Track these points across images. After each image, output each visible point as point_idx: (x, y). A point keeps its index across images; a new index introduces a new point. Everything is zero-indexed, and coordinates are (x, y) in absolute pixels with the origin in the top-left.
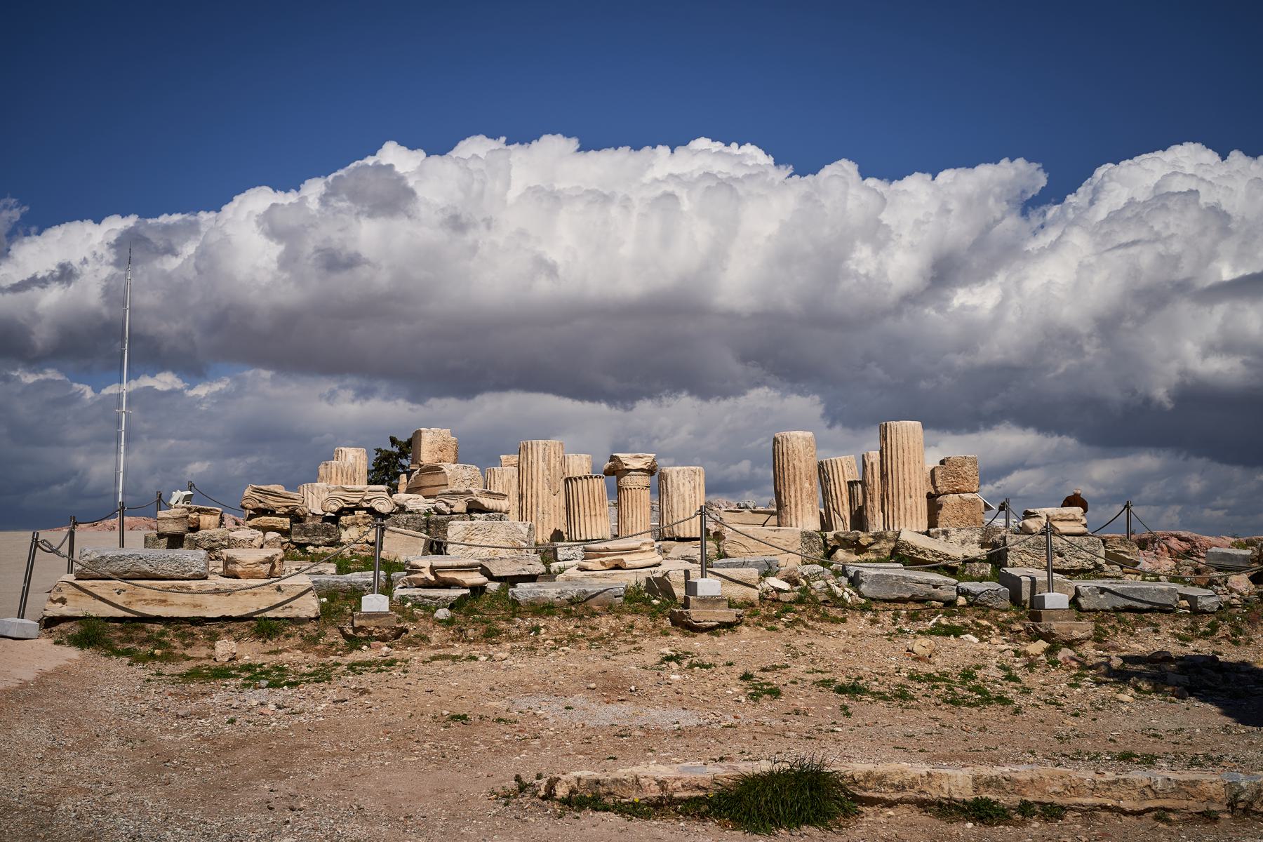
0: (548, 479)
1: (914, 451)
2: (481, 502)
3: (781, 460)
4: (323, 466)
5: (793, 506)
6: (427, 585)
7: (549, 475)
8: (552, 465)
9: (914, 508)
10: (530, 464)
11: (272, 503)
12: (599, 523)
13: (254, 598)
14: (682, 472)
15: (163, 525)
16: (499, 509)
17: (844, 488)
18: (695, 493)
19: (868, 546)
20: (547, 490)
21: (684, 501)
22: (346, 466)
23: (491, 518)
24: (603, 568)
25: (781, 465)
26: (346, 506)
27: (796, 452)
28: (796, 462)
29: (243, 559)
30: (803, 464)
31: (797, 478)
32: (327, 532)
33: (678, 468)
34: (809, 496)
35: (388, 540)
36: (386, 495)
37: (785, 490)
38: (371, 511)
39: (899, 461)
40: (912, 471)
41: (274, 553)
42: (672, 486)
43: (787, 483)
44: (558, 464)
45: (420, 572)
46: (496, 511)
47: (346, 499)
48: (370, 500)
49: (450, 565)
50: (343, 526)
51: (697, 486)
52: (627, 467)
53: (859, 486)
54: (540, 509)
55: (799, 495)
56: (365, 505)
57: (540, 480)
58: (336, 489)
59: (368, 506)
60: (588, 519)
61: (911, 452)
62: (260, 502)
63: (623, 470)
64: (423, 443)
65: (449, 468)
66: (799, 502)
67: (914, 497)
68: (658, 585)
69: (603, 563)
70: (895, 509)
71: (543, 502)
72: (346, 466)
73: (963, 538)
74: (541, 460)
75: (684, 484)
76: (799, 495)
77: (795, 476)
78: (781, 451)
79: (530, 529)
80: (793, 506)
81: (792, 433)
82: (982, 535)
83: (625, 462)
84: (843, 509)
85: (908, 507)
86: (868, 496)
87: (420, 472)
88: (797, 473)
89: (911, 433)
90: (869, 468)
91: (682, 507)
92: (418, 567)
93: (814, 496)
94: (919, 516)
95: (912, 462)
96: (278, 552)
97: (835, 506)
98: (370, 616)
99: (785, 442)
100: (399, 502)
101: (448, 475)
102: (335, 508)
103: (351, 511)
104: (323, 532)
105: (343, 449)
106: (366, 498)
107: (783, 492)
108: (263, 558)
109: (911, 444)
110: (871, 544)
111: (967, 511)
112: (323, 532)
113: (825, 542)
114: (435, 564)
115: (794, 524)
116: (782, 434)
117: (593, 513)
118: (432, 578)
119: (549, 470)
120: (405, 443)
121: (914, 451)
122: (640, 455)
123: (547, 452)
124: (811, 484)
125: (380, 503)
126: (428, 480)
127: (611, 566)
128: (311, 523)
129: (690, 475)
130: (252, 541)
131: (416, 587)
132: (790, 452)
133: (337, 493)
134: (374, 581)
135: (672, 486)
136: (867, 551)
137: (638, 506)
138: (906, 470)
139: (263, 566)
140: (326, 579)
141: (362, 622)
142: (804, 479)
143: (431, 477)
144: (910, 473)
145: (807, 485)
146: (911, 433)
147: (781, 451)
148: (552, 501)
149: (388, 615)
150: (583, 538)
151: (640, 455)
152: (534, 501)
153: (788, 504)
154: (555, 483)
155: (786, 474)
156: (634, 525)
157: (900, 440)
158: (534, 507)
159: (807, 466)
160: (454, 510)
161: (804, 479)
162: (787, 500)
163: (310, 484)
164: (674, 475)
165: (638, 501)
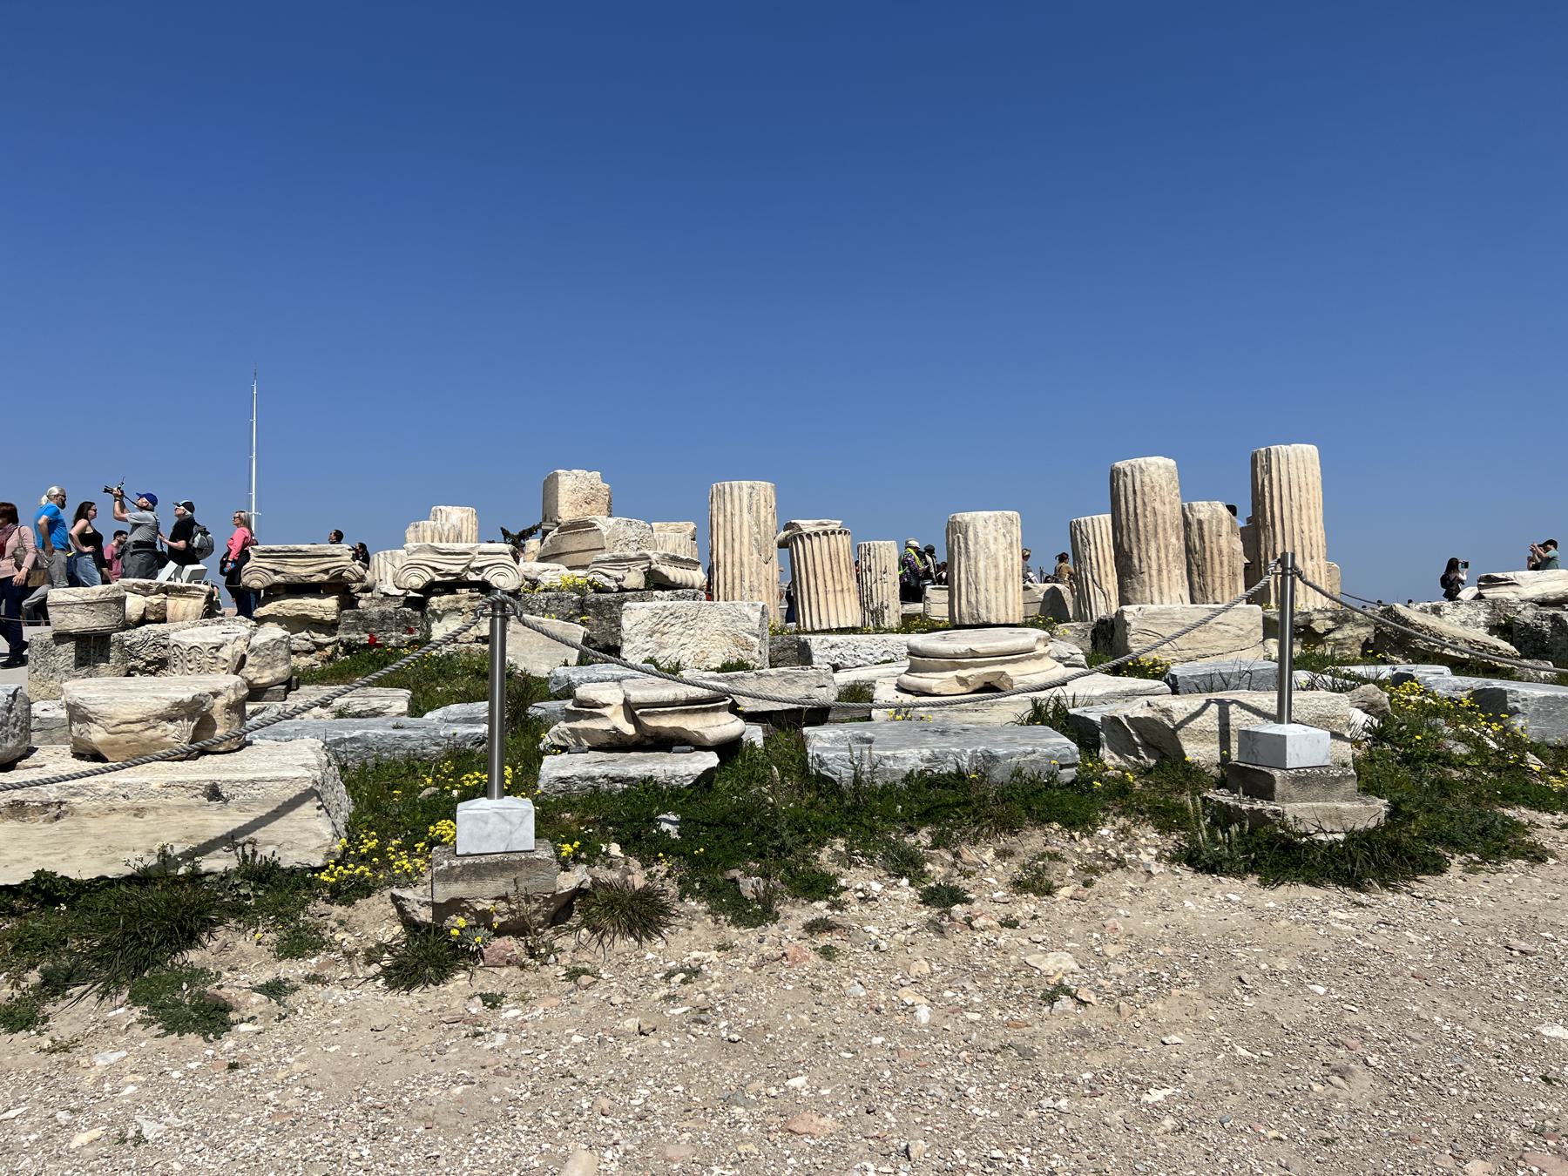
0: (756, 540)
2: (665, 573)
4: (411, 528)
5: (1154, 573)
6: (615, 744)
7: (759, 533)
8: (762, 519)
10: (729, 516)
11: (295, 570)
12: (847, 602)
13: (138, 825)
14: (993, 519)
15: (61, 616)
16: (690, 584)
18: (1012, 553)
20: (756, 555)
21: (996, 566)
22: (446, 528)
23: (684, 597)
24: (964, 690)
25: (1131, 510)
26: (438, 579)
27: (1157, 489)
28: (1158, 505)
29: (104, 709)
30: (1168, 507)
31: (1160, 530)
32: (406, 624)
33: (986, 514)
35: (515, 638)
36: (509, 559)
37: (1139, 549)
38: (485, 587)
41: (205, 689)
42: (976, 543)
43: (1142, 538)
44: (770, 517)
45: (600, 716)
46: (686, 587)
47: (439, 566)
48: (481, 569)
49: (671, 697)
50: (434, 612)
51: (1015, 542)
54: (746, 584)
55: (1163, 555)
56: (472, 577)
57: (746, 541)
58: (420, 550)
59: (479, 578)
60: (831, 596)
62: (276, 572)
65: (604, 523)
66: (1164, 566)
67: (1315, 559)
68: (1140, 735)
69: (962, 681)
71: (751, 573)
72: (446, 528)
73: (1463, 618)
74: (745, 510)
75: (996, 539)
76: (1163, 555)
77: (1156, 527)
78: (1130, 489)
79: (763, 613)
80: (1154, 573)
81: (1149, 459)
82: (1489, 614)
84: (1107, 582)
86: (1195, 568)
87: (559, 532)
88: (1160, 521)
89: (1309, 462)
90: (1195, 527)
92: (595, 705)
95: (1312, 506)
96: (220, 687)
97: (1096, 577)
98: (479, 870)
99: (1137, 474)
100: (529, 575)
101: (605, 534)
102: (418, 582)
103: (450, 587)
104: (398, 625)
105: (442, 508)
106: (474, 565)
107: (1135, 551)
108: (167, 703)
110: (1329, 631)
112: (398, 625)
114: (637, 696)
115: (1156, 599)
116: (1132, 461)
117: (838, 588)
118: (629, 729)
119: (758, 526)
120: (517, 536)
122: (825, 521)
124: (1178, 539)
125: (500, 574)
126: (572, 543)
127: (977, 687)
128: (377, 609)
129: (1005, 524)
130: (218, 649)
131: (591, 749)
132: (1147, 489)
133: (422, 556)
134: (491, 729)
135: (976, 543)
138: (1305, 517)
139: (171, 727)
140: (380, 732)
141: (458, 889)
142: (1170, 531)
143: (578, 538)
144: (1310, 523)
145: (1174, 540)
146: (1309, 462)
147: (1130, 489)
148: (763, 572)
149: (531, 863)
150: (825, 626)
151: (825, 521)
152: (737, 571)
153: (1145, 569)
154: (767, 545)
155: (1140, 523)
158: (737, 582)
160: (625, 584)
162: (1144, 564)
163: (388, 552)
164: (980, 525)
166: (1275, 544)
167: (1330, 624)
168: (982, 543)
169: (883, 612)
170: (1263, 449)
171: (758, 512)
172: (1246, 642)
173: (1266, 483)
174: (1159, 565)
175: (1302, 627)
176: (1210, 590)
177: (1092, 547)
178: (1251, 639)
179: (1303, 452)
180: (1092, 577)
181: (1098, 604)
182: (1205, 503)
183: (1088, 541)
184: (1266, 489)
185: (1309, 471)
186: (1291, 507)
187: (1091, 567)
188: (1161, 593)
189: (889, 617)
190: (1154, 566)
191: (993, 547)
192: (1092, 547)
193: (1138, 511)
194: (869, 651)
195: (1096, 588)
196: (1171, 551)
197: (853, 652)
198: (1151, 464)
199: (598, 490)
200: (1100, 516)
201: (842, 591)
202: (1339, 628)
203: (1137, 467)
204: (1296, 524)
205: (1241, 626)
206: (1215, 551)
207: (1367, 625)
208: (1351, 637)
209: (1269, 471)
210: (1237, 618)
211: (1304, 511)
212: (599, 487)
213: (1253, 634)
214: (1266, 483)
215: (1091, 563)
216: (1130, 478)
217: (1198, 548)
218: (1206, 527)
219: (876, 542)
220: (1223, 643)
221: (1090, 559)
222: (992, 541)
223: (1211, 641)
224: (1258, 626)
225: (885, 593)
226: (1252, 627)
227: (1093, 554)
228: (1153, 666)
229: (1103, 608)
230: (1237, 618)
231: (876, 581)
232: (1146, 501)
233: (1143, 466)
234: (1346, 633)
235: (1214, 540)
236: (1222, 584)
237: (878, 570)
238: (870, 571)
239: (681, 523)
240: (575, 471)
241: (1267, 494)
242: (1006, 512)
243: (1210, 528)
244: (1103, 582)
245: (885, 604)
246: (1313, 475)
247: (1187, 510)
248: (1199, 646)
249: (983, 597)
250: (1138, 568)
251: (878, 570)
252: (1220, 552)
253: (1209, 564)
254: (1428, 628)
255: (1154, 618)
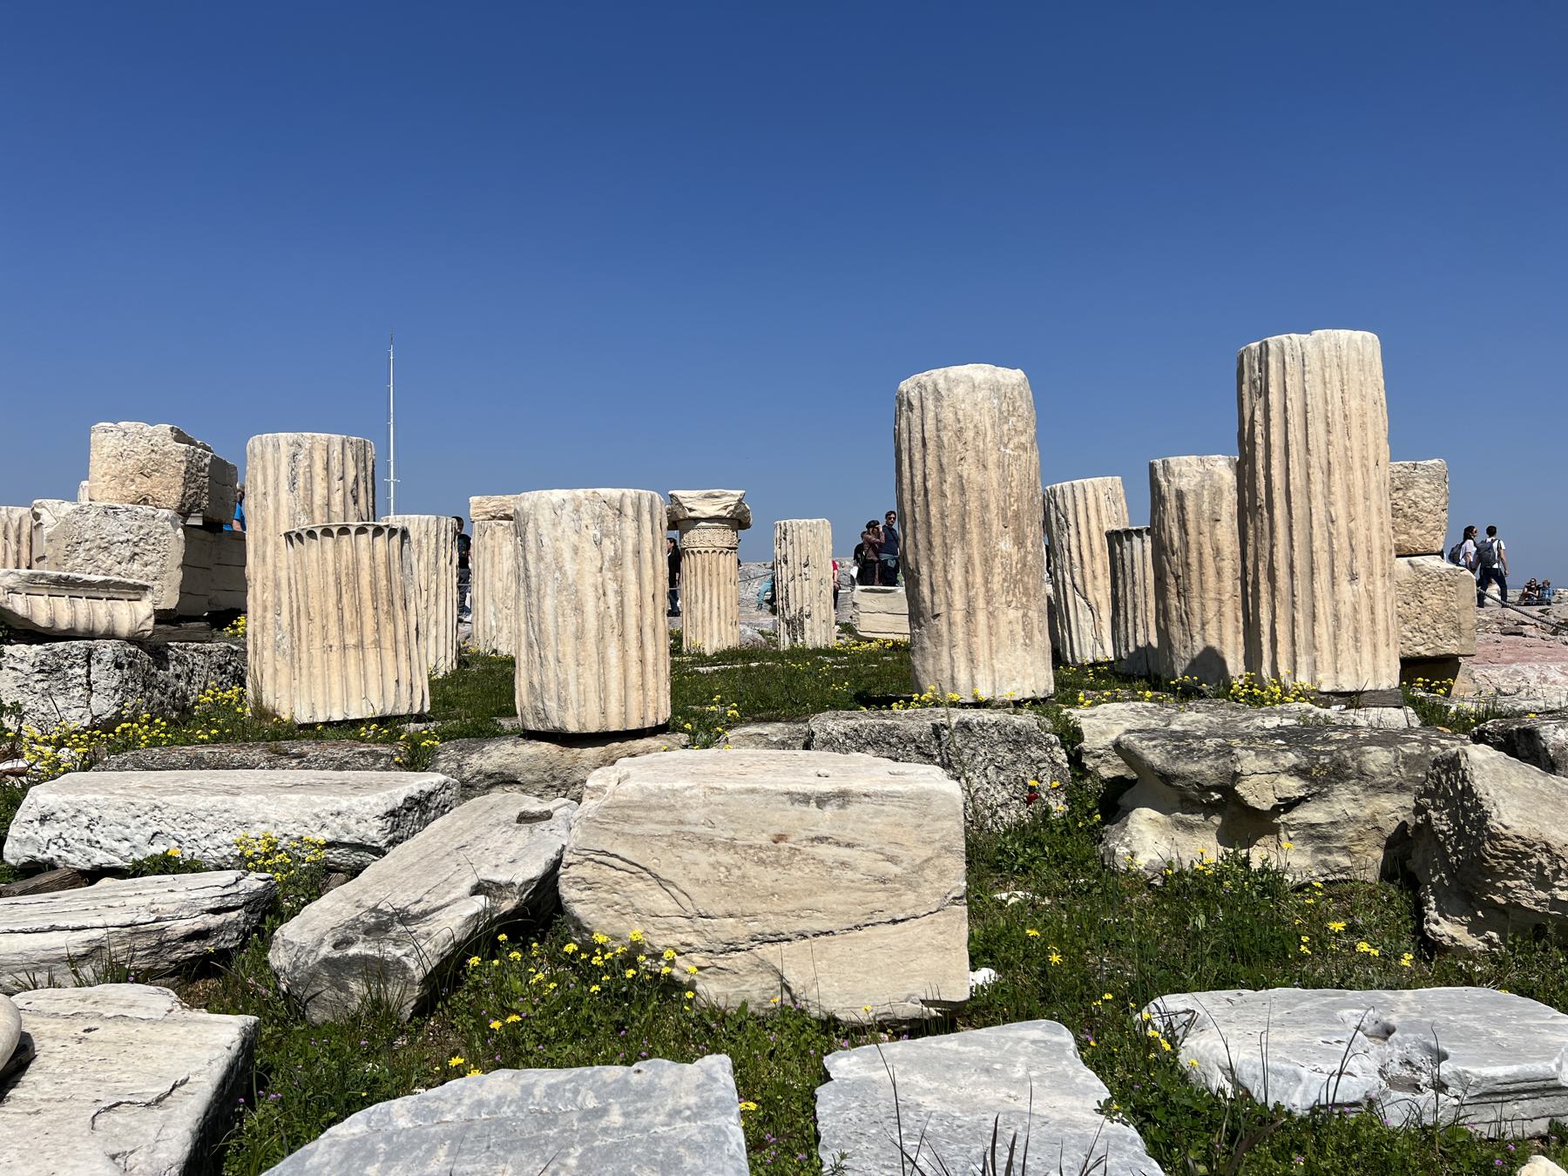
1: (1363, 426)
3: (918, 466)
5: (958, 617)
8: (318, 500)
9: (1364, 615)
14: (569, 508)
17: (1100, 545)
19: (1276, 810)
21: (579, 609)
25: (918, 480)
28: (969, 470)
33: (558, 495)
34: (1012, 581)
37: (931, 564)
39: (1314, 461)
40: (1358, 492)
42: (540, 559)
43: (937, 541)
44: (337, 498)
51: (629, 558)
52: (692, 514)
53: (1148, 538)
61: (1355, 432)
63: (685, 519)
64: (94, 456)
67: (1363, 578)
70: (1300, 617)
74: (284, 485)
75: (576, 550)
76: (979, 579)
77: (964, 515)
80: (958, 617)
81: (955, 371)
83: (689, 505)
84: (1095, 588)
85: (1345, 610)
86: (1171, 580)
88: (973, 505)
89: (1354, 370)
90: (1171, 505)
91: (571, 629)
93: (1031, 582)
94: (1381, 637)
95: (1357, 464)
97: (1078, 581)
99: (930, 404)
107: (924, 570)
109: (1354, 404)
110: (1290, 804)
111: (1434, 601)
113: (1076, 759)
117: (351, 640)
121: (1363, 426)
123: (303, 463)
124: (1019, 542)
129: (601, 518)
132: (946, 436)
135: (540, 559)
136: (1274, 830)
137: (715, 584)
142: (996, 526)
144: (1350, 501)
145: (1006, 545)
146: (1354, 370)
151: (716, 492)
153: (941, 609)
155: (934, 510)
156: (707, 615)
157: (1314, 388)
159: (1005, 481)
161: (996, 526)
162: (939, 598)
164: (545, 518)
165: (715, 574)
166: (1272, 546)
167: (1292, 786)
168: (549, 558)
169: (802, 623)
170: (1255, 345)
171: (310, 490)
172: (909, 898)
173: (1259, 416)
174: (970, 602)
175: (1217, 789)
176: (1197, 622)
177: (1073, 531)
178: (926, 890)
179: (1338, 346)
180: (1073, 578)
181: (1081, 623)
182: (1193, 459)
183: (1067, 521)
184: (1259, 429)
185: (1353, 388)
186: (1308, 466)
187: (1071, 564)
188: (972, 660)
189: (812, 630)
190: (959, 602)
191: (569, 567)
192: (1073, 531)
193: (929, 484)
194: (118, 831)
195: (1078, 598)
196: (998, 569)
197: (86, 834)
198: (957, 382)
199: (165, 454)
200: (1087, 481)
201: (360, 645)
202: (1319, 796)
203: (930, 388)
204: (1318, 504)
205: (891, 850)
206: (1208, 551)
207: (1401, 788)
208: (1354, 820)
209: (1265, 392)
210: (879, 823)
211: (1337, 476)
212: (166, 449)
213: (930, 874)
214: (1259, 416)
215: (1070, 557)
216: (917, 412)
217: (1176, 544)
218: (1190, 504)
219: (794, 521)
220: (831, 899)
221: (1069, 550)
222: (567, 555)
223: (794, 894)
224: (948, 850)
225: (806, 595)
226: (927, 852)
227: (1074, 542)
228: (629, 960)
229: (1088, 631)
230: (879, 823)
231: (793, 579)
232: (945, 461)
233: (942, 385)
234: (1338, 808)
235: (1206, 528)
236: (1220, 613)
237: (797, 561)
238: (786, 562)
239: (507, 498)
240: (122, 424)
241: (1259, 440)
242: (602, 491)
243: (1199, 507)
244: (1089, 587)
245: (806, 610)
246: (1363, 397)
247: (1160, 472)
248: (758, 906)
249: (551, 674)
250: (928, 604)
251: (797, 561)
252: (1217, 552)
253: (1194, 576)
254: (1548, 849)
255: (627, 819)
